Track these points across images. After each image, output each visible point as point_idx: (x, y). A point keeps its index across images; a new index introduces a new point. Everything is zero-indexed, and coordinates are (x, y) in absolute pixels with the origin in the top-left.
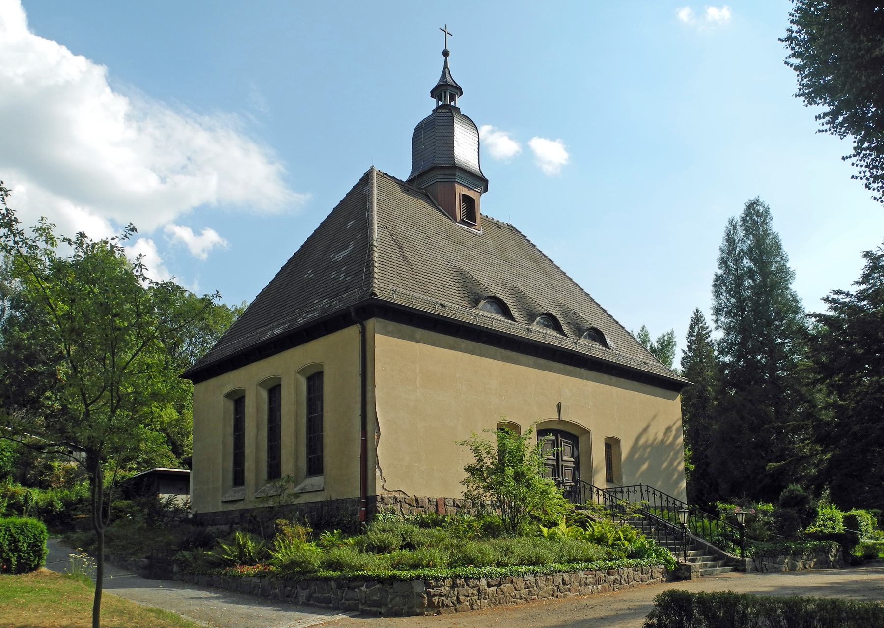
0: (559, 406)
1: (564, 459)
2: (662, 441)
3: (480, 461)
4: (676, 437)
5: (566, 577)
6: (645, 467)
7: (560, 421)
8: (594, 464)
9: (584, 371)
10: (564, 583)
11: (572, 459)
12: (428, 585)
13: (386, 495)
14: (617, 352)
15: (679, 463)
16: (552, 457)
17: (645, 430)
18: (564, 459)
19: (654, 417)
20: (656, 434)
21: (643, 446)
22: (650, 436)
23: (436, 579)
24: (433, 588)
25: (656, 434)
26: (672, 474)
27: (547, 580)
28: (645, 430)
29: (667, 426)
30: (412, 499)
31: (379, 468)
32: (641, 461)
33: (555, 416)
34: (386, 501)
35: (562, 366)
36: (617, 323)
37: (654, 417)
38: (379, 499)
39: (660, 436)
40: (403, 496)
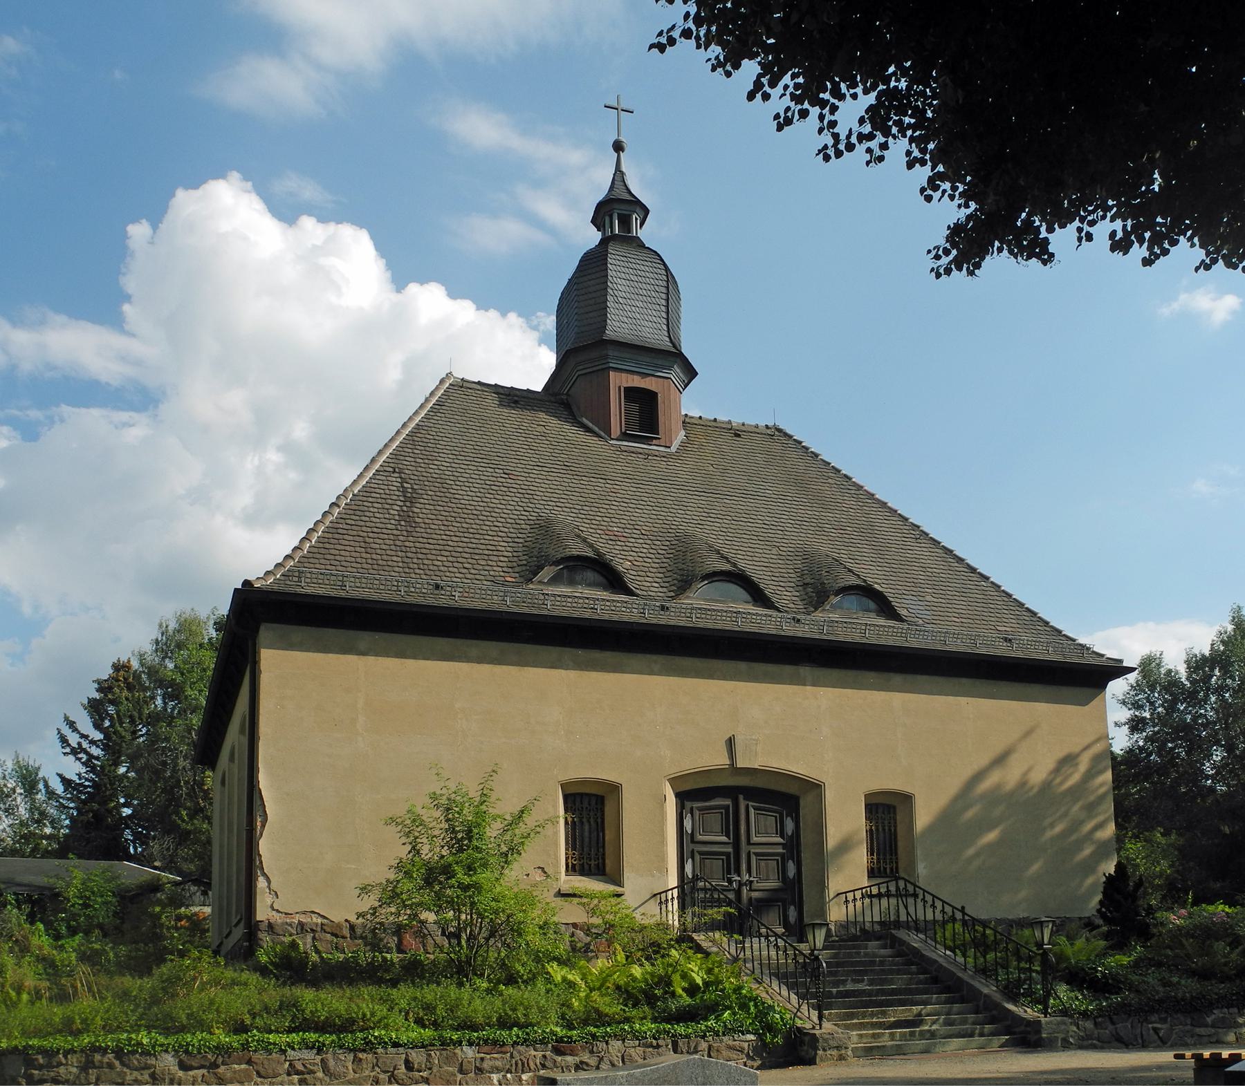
0: (730, 743)
1: (755, 839)
2: (1047, 786)
3: (415, 850)
4: (1091, 774)
5: (417, 1057)
6: (992, 836)
7: (734, 770)
8: (833, 837)
9: (805, 671)
10: (409, 1065)
11: (779, 840)
12: (30, 1063)
13: (277, 918)
14: (929, 624)
15: (1100, 826)
16: (724, 839)
17: (1000, 760)
18: (755, 839)
19: (1028, 734)
20: (1030, 770)
21: (983, 796)
22: (1009, 776)
23: (49, 1053)
24: (40, 1067)
25: (1030, 770)
26: (1079, 844)
27: (357, 1061)
28: (1000, 760)
29: (1061, 754)
30: (339, 926)
31: (264, 874)
32: (983, 825)
33: (722, 760)
34: (278, 930)
35: (743, 666)
36: (973, 570)
37: (1028, 734)
38: (263, 926)
39: (1038, 776)
40: (320, 921)
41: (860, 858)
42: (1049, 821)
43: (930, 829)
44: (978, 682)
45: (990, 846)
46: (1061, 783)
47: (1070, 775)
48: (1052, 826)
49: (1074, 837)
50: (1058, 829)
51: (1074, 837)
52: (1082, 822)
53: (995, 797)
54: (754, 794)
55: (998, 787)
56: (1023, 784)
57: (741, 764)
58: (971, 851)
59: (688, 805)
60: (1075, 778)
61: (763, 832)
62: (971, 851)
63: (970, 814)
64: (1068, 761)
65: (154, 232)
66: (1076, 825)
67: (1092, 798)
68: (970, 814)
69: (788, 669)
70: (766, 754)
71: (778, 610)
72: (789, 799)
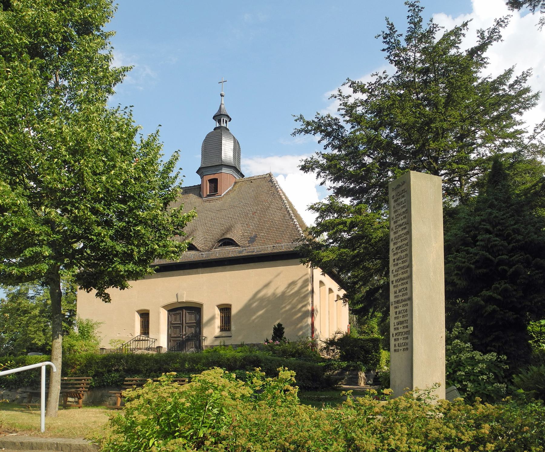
2: (284, 293)
20: (277, 288)
22: (269, 292)
26: (296, 313)
28: (267, 285)
29: (290, 281)
39: (279, 291)
41: (218, 322)
42: (284, 305)
43: (240, 311)
44: (256, 264)
45: (260, 316)
46: (289, 292)
47: (293, 288)
48: (285, 307)
49: (294, 310)
50: (287, 308)
51: (294, 310)
52: (297, 305)
53: (262, 299)
54: (187, 308)
55: (265, 295)
56: (274, 294)
57: (179, 301)
58: (254, 317)
59: (171, 313)
60: (296, 289)
61: (189, 318)
62: (254, 317)
63: (255, 305)
64: (293, 283)
65: (279, 174)
66: (293, 307)
67: (303, 295)
68: (255, 305)
69: (195, 270)
70: (187, 297)
71: (197, 250)
72: (196, 309)
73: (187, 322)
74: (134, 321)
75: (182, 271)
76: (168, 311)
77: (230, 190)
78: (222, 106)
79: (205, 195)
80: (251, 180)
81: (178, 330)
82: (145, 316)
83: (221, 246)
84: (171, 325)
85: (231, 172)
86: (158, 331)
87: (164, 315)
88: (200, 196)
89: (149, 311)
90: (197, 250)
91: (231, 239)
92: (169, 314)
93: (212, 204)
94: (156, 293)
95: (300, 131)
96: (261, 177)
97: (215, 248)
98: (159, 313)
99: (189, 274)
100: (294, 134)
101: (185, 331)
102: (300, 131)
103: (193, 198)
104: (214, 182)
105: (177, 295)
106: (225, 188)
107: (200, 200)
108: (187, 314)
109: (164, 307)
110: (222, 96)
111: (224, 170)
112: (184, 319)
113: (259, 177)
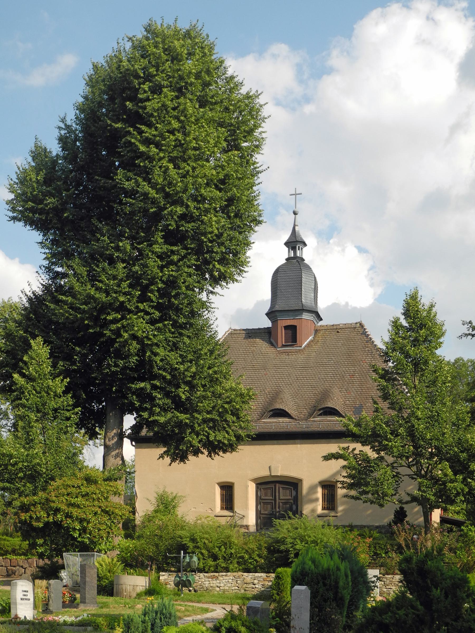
59: (260, 486)
61: (284, 494)
70: (281, 470)
71: (292, 418)
72: (293, 484)
73: (281, 498)
74: (214, 494)
75: (275, 442)
76: (256, 484)
77: (312, 341)
78: (297, 228)
79: (280, 344)
80: (336, 329)
81: (269, 506)
82: (228, 490)
83: (320, 415)
84: (259, 500)
85: (312, 318)
86: (246, 507)
87: (252, 487)
88: (273, 345)
89: (233, 484)
90: (292, 418)
91: (334, 409)
92: (257, 488)
93: (293, 357)
94: (248, 465)
95: (467, 335)
96: (350, 326)
97: (314, 417)
98: (247, 487)
99: (283, 444)
100: (461, 337)
101: (279, 508)
102: (467, 335)
103: (261, 344)
104: (292, 330)
105: (270, 467)
106: (306, 340)
107: (273, 349)
108: (281, 489)
109: (254, 480)
110: (295, 213)
111: (306, 316)
112: (277, 494)
113: (347, 326)
